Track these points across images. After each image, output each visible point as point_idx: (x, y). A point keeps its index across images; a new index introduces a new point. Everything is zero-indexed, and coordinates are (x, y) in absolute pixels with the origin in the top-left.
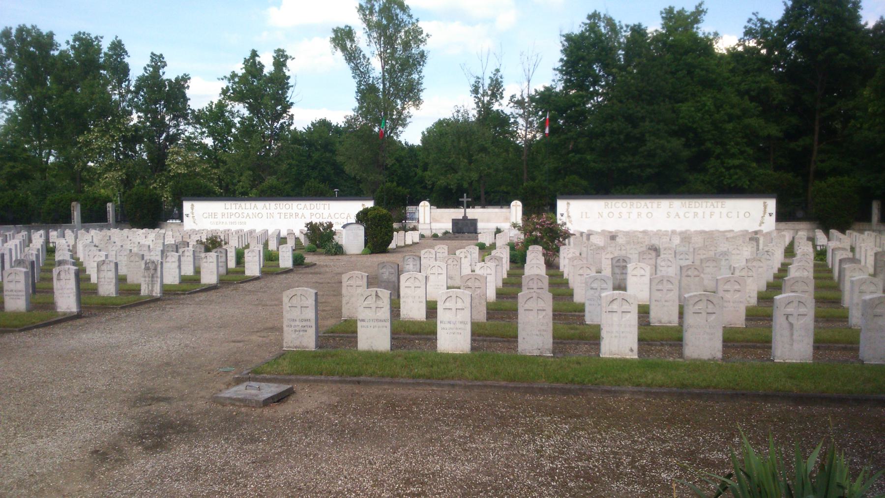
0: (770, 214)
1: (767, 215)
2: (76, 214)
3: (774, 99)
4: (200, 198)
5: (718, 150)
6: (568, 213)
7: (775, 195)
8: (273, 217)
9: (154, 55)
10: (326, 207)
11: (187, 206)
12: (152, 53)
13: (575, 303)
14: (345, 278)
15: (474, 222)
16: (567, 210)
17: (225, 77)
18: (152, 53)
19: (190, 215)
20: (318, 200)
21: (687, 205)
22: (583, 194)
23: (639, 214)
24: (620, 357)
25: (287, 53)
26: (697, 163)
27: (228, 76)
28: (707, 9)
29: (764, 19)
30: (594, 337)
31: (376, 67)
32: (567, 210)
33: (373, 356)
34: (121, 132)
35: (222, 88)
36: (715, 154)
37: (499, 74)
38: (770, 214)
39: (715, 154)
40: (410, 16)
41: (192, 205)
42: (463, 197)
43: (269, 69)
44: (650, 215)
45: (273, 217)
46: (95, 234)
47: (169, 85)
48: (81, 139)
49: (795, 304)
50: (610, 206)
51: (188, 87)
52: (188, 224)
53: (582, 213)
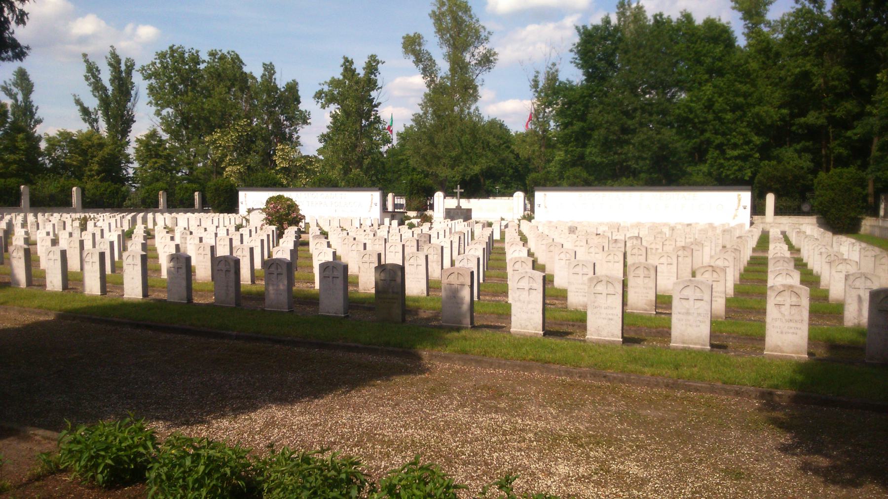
1: (741, 208)
2: (162, 200)
3: (814, 85)
5: (719, 139)
7: (750, 187)
9: (266, 65)
12: (264, 64)
13: (556, 289)
15: (469, 211)
17: (326, 82)
18: (264, 64)
19: (244, 203)
22: (583, 186)
24: (699, 347)
25: (379, 58)
26: (699, 154)
27: (328, 81)
28: (112, 47)
30: (580, 321)
31: (443, 67)
33: (525, 340)
34: (238, 132)
36: (714, 144)
37: (556, 67)
39: (714, 144)
40: (470, 16)
42: (461, 188)
43: (361, 72)
46: (184, 219)
48: (207, 139)
49: (526, 279)
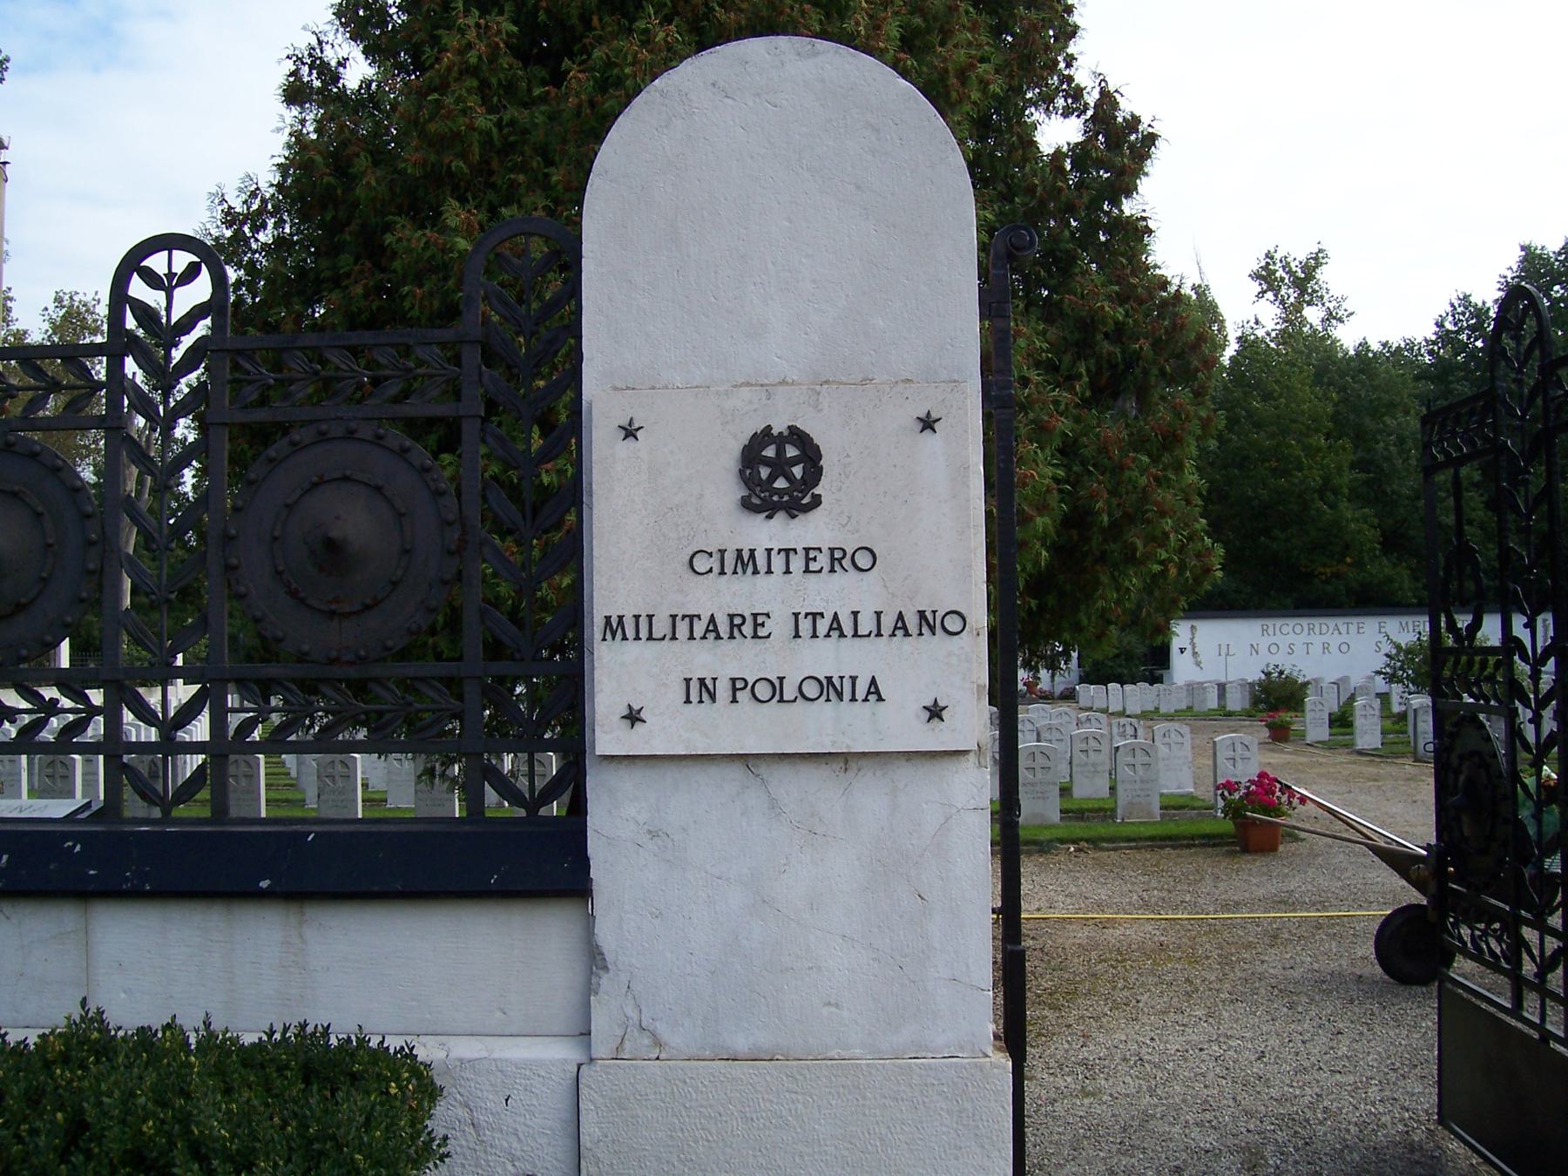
0: (1181, 649)
4: (1301, 611)
6: (1194, 647)
8: (1257, 653)
10: (1353, 628)
11: (1181, 633)
14: (232, 758)
16: (1192, 639)
20: (1385, 614)
21: (1317, 630)
23: (1326, 647)
29: (1217, 307)
32: (1192, 639)
35: (769, 428)
38: (1181, 649)
41: (1193, 627)
44: (1344, 648)
45: (1257, 653)
47: (1088, 374)
50: (1271, 631)
51: (1385, 345)
52: (1182, 669)
53: (1220, 645)
